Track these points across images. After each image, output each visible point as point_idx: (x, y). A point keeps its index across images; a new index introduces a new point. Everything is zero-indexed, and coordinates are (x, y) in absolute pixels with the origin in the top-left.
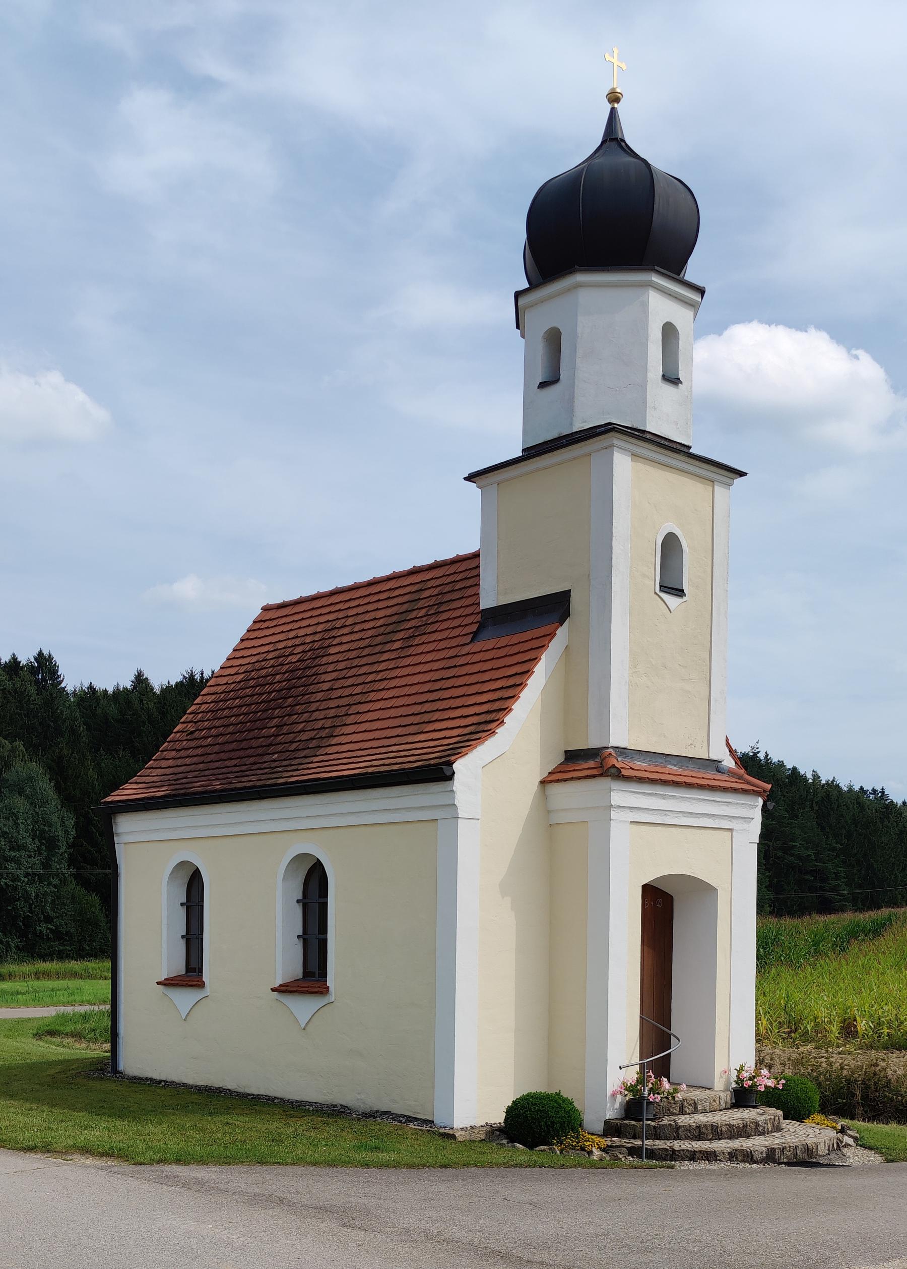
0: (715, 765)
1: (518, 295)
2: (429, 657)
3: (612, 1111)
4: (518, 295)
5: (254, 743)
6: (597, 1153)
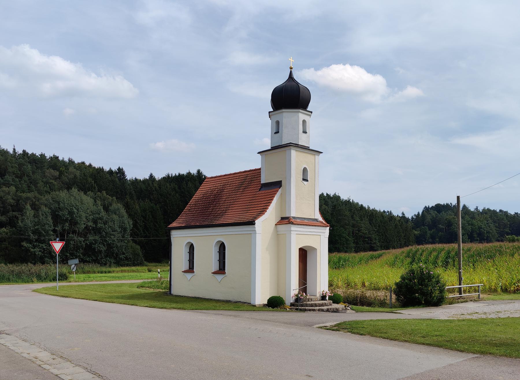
0: (316, 220)
1: (269, 112)
2: (249, 194)
3: (292, 301)
4: (269, 112)
5: (206, 213)
6: (288, 309)
